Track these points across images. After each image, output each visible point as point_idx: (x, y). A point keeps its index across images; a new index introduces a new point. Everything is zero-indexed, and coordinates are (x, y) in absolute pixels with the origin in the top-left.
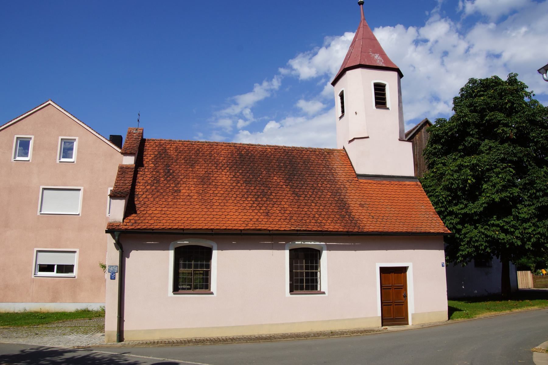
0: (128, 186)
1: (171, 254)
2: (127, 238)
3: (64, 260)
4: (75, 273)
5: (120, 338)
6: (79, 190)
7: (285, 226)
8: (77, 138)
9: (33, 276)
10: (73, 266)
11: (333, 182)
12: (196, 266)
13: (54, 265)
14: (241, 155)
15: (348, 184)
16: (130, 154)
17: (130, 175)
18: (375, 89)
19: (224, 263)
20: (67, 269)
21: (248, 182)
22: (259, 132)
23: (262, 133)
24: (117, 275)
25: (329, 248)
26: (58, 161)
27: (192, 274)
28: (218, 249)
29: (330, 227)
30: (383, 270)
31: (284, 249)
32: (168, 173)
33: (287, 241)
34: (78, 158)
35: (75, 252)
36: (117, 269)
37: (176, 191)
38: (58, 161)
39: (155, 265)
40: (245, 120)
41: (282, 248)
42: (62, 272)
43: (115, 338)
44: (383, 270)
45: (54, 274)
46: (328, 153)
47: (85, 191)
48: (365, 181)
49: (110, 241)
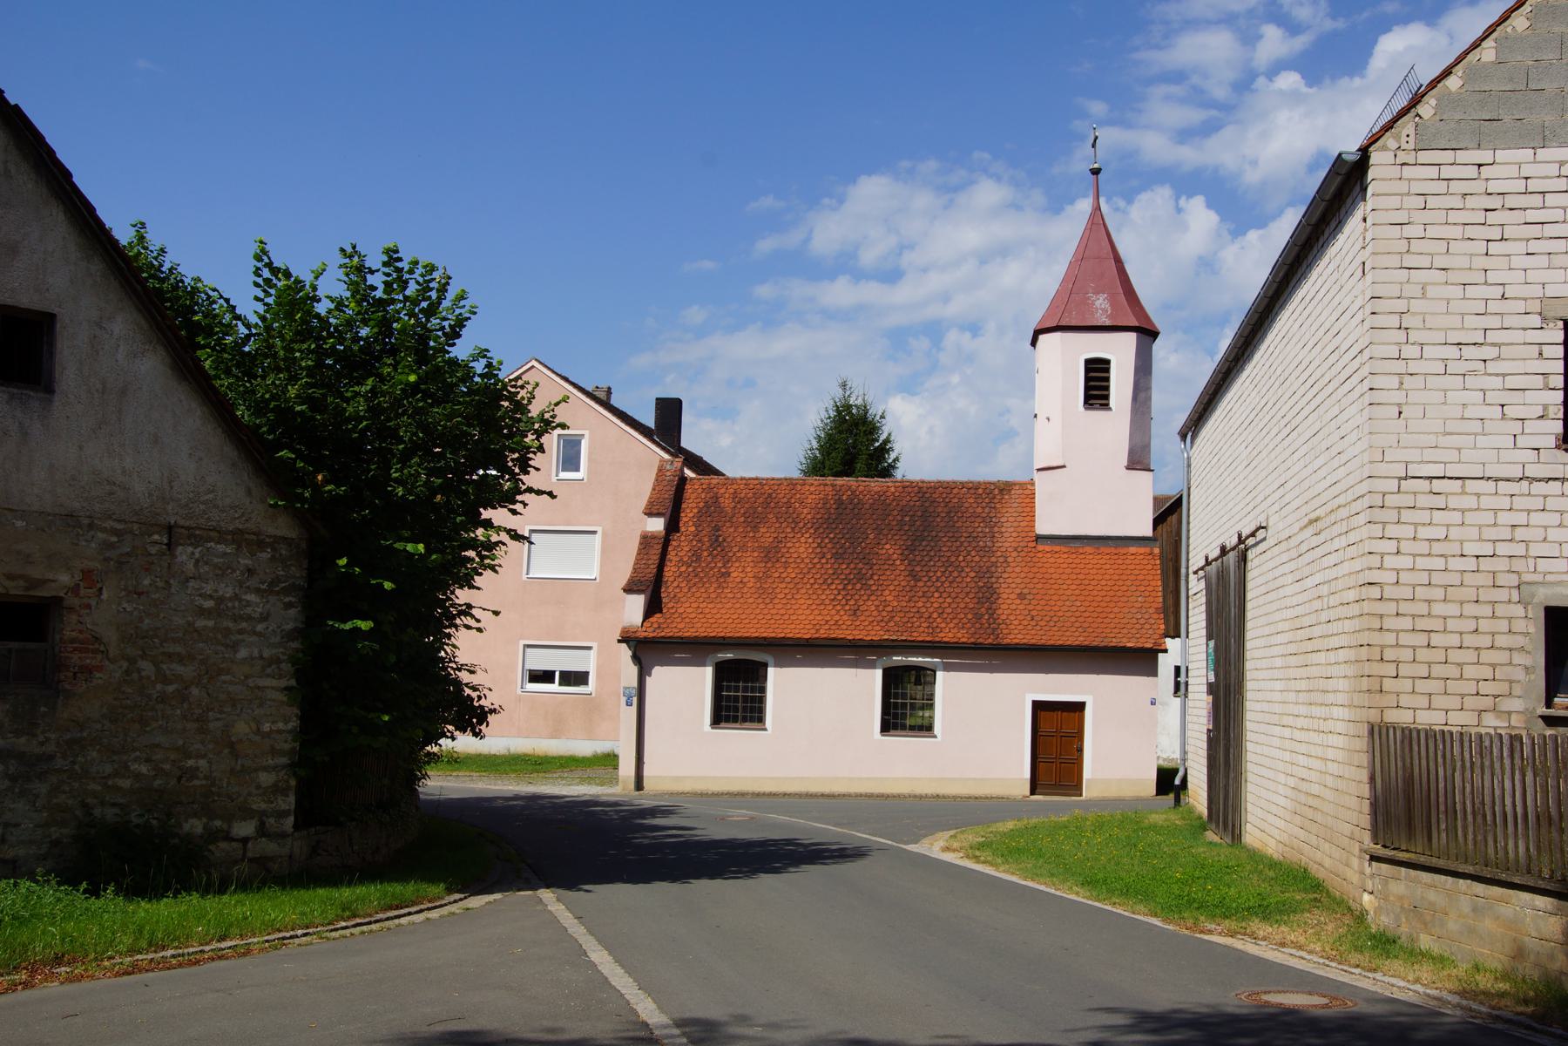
0: (653, 568)
1: (708, 672)
2: (648, 650)
3: (571, 661)
4: (591, 687)
5: (639, 784)
6: (594, 532)
7: (876, 634)
8: (586, 433)
9: (519, 691)
10: (587, 674)
11: (988, 551)
12: (745, 689)
13: (553, 673)
14: (840, 502)
15: (1015, 554)
16: (658, 515)
17: (657, 549)
18: (1087, 370)
19: (783, 685)
20: (575, 678)
21: (837, 556)
22: (1346, 79)
23: (1357, 81)
24: (635, 700)
25: (948, 668)
26: (554, 479)
27: (738, 702)
28: (776, 666)
29: (948, 635)
30: (1038, 706)
31: (874, 667)
32: (717, 542)
33: (880, 656)
34: (590, 471)
35: (589, 648)
36: (634, 692)
37: (723, 575)
38: (554, 479)
39: (686, 688)
40: (1292, 28)
41: (872, 665)
42: (569, 684)
43: (632, 786)
44: (1038, 706)
45: (554, 687)
46: (1001, 491)
47: (604, 534)
48: (1048, 548)
49: (625, 652)
